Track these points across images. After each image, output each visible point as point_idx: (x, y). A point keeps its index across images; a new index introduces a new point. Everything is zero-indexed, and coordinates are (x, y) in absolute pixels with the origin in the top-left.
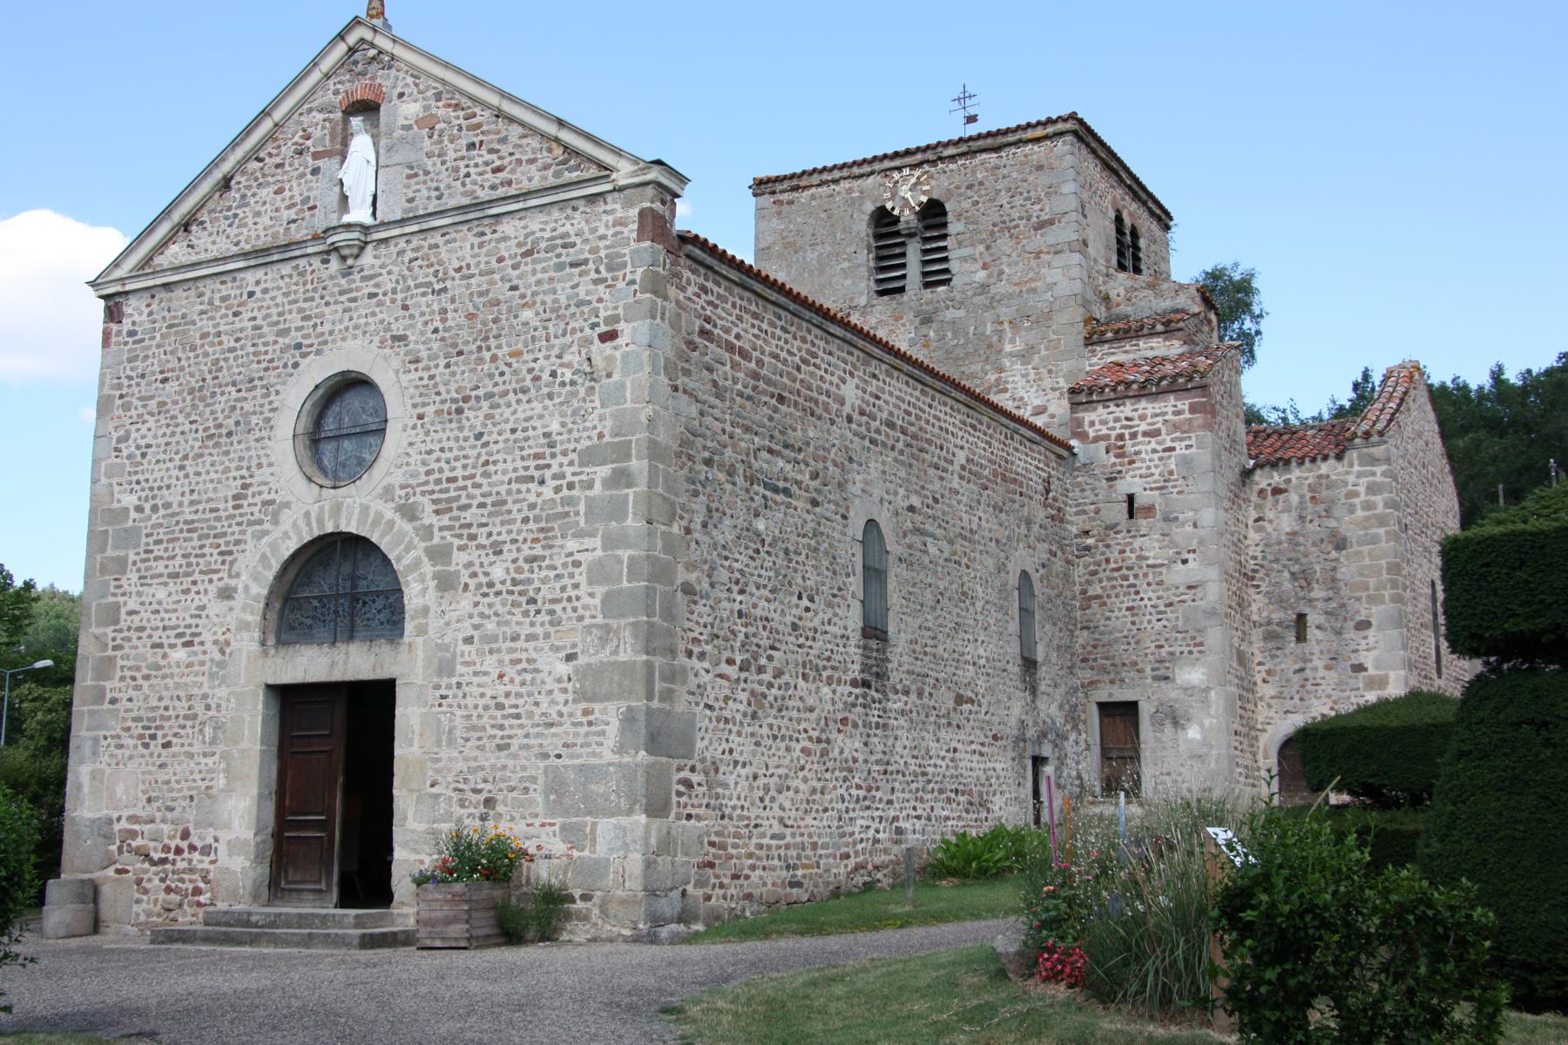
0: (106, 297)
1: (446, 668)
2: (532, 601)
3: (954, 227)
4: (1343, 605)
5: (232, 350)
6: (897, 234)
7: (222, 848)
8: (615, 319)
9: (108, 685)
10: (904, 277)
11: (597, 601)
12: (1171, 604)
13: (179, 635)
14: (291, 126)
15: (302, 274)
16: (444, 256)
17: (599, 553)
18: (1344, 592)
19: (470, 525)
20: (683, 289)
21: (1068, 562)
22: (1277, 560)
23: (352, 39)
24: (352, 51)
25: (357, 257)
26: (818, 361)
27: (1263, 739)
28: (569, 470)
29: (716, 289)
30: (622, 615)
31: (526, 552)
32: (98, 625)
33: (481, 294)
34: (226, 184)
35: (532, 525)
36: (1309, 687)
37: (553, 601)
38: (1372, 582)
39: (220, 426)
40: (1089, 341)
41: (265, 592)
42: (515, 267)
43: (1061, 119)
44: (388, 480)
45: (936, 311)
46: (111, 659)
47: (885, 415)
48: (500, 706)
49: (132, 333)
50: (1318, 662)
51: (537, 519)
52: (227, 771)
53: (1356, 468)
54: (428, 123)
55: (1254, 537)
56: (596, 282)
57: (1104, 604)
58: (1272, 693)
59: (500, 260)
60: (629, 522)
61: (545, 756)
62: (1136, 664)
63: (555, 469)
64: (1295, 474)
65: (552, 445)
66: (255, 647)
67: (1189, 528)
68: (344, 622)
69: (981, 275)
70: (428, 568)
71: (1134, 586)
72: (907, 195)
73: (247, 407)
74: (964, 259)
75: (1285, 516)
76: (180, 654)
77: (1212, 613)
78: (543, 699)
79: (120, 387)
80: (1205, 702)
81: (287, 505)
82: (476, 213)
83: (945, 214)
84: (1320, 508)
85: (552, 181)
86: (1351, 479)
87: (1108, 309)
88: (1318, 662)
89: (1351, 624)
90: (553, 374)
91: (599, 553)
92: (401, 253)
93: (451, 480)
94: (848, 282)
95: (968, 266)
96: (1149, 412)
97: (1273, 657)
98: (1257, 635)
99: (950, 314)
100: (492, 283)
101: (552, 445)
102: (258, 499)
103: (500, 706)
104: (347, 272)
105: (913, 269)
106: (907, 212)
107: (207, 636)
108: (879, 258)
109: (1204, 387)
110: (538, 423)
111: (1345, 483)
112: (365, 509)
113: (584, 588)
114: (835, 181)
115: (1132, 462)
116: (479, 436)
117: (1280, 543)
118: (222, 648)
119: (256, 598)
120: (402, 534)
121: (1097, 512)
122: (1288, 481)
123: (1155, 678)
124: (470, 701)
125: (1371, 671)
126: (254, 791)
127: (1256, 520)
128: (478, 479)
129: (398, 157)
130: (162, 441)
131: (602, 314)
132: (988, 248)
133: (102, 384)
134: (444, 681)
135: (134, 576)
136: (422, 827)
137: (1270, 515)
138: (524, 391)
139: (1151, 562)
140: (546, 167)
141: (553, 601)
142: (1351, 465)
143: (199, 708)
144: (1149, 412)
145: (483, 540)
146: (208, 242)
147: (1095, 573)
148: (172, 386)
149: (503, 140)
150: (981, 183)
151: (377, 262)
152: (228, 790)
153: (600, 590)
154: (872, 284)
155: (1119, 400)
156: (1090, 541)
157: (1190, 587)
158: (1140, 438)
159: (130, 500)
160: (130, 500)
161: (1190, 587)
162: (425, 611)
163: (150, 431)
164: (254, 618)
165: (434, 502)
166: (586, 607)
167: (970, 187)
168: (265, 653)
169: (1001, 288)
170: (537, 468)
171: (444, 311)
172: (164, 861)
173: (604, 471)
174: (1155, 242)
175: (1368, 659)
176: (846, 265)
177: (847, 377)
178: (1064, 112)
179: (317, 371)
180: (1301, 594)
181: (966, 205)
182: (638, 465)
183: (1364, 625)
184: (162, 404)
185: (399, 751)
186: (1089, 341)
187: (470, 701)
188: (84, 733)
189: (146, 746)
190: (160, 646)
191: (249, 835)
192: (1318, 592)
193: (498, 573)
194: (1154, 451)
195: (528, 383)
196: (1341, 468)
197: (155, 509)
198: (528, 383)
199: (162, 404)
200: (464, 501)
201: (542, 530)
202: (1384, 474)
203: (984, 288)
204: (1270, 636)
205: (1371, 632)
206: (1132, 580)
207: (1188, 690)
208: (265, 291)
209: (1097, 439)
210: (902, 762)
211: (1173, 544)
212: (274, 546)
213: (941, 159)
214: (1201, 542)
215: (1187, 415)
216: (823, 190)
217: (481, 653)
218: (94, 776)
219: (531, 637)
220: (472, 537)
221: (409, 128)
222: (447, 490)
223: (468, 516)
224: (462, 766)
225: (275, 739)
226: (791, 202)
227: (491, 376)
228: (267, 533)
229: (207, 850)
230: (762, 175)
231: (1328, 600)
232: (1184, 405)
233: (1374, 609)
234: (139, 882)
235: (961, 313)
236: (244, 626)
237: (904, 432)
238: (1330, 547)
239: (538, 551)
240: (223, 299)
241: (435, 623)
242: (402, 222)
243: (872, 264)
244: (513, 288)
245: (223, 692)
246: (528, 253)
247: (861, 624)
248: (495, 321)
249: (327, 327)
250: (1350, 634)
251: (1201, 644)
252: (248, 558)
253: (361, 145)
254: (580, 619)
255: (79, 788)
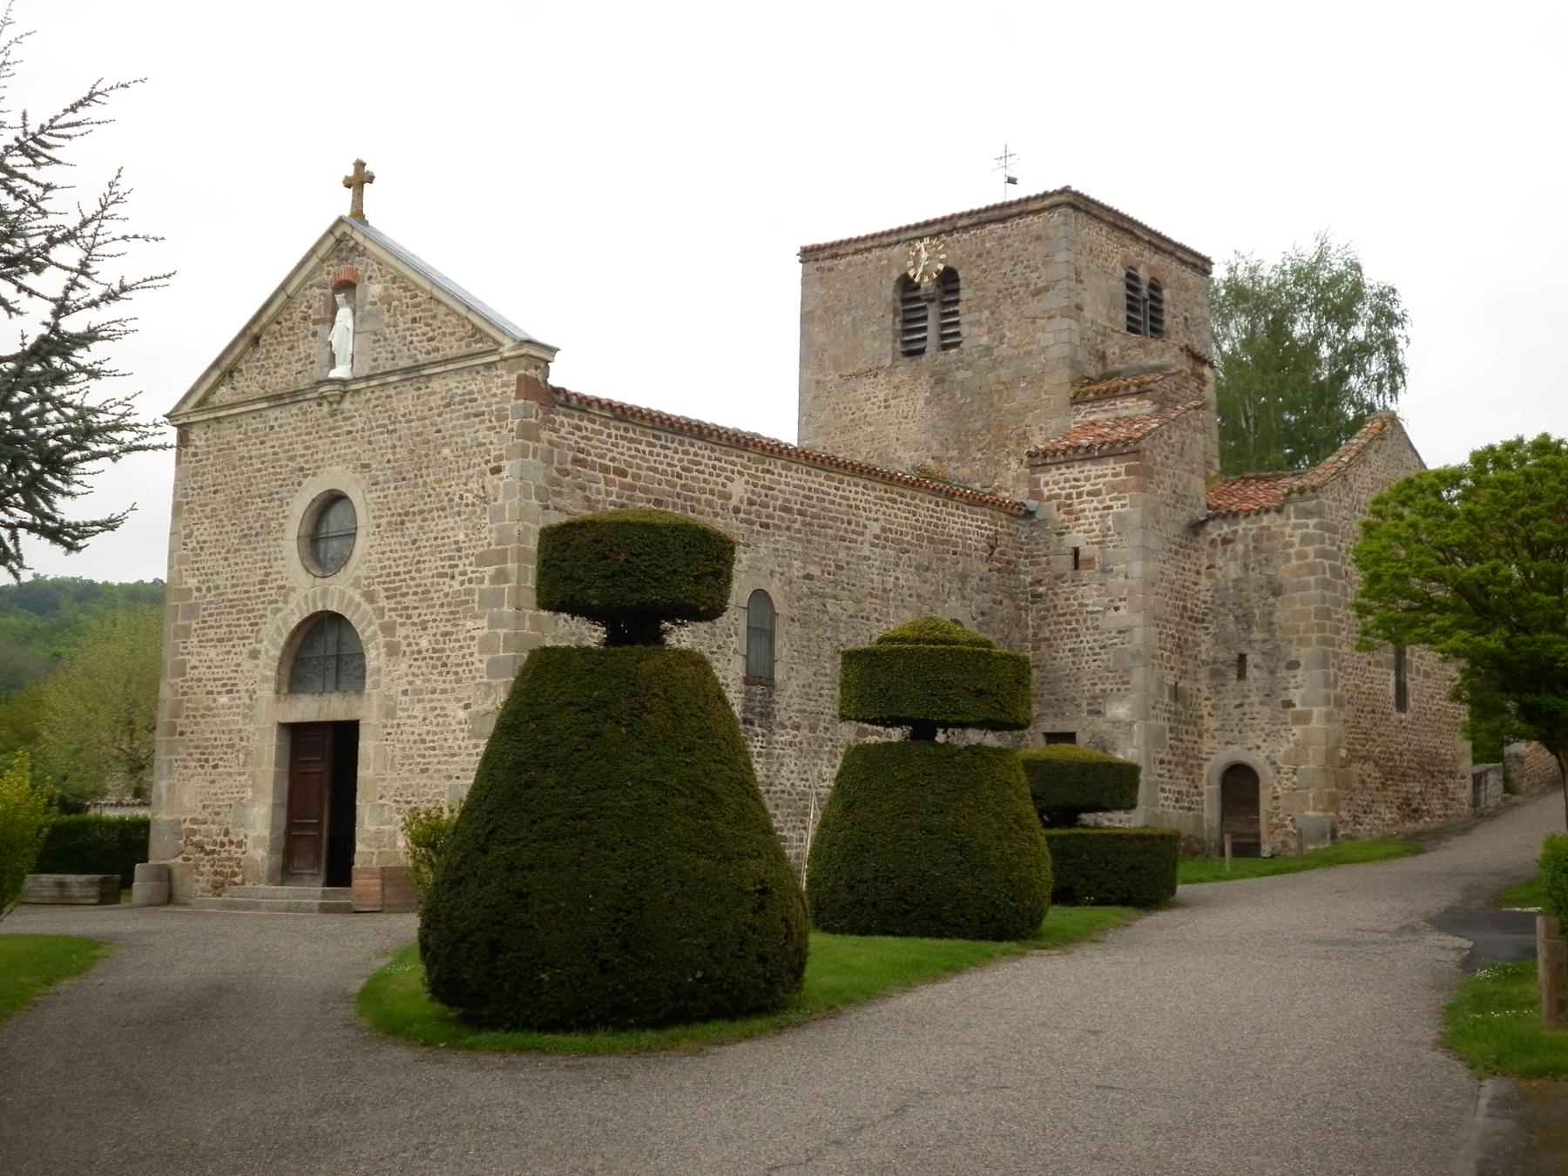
0: (178, 426)
1: (390, 713)
2: (444, 665)
3: (966, 293)
4: (1277, 647)
5: (259, 470)
6: (918, 299)
7: (249, 842)
8: (499, 458)
9: (179, 721)
10: (925, 339)
11: (484, 666)
12: (1104, 647)
13: (224, 685)
14: (299, 299)
15: (304, 414)
16: (395, 404)
17: (486, 631)
18: (1279, 634)
19: (407, 608)
20: (556, 431)
21: (1019, 608)
22: (1223, 605)
23: (338, 234)
24: (339, 241)
25: (339, 403)
26: (701, 468)
27: (1206, 767)
28: (469, 569)
29: (590, 426)
30: (498, 677)
31: (442, 629)
32: (173, 676)
33: (418, 435)
34: (256, 340)
35: (446, 609)
36: (1247, 721)
37: (458, 665)
38: (1302, 625)
39: (250, 528)
40: (1076, 401)
41: (278, 654)
42: (440, 415)
43: (1055, 193)
44: (358, 573)
45: (949, 371)
46: (180, 702)
47: (779, 503)
48: (423, 741)
49: (195, 455)
50: (1255, 699)
51: (449, 604)
52: (253, 786)
53: (1293, 520)
54: (387, 299)
55: (1205, 582)
56: (490, 429)
57: (1051, 646)
58: (1216, 725)
59: (430, 409)
60: (505, 608)
61: (450, 777)
62: (1074, 699)
63: (461, 568)
64: (1242, 526)
65: (459, 550)
66: (271, 694)
67: (1121, 579)
68: (331, 676)
69: (985, 340)
70: (381, 639)
71: (1074, 630)
72: (925, 263)
73: (269, 514)
74: (972, 324)
75: (1232, 565)
76: (223, 699)
77: (1136, 655)
78: (449, 736)
79: (186, 496)
80: (1130, 734)
81: (293, 589)
82: (413, 373)
83: (958, 280)
84: (1262, 556)
85: (464, 351)
86: (1288, 530)
87: (1105, 366)
88: (1255, 699)
89: (1282, 664)
90: (461, 497)
91: (486, 631)
92: (368, 401)
93: (397, 574)
94: (877, 344)
95: (975, 330)
96: (1092, 474)
97: (1218, 692)
98: (1204, 673)
99: (960, 375)
100: (425, 426)
101: (459, 550)
102: (275, 585)
103: (423, 741)
104: (333, 414)
105: (932, 334)
106: (926, 279)
107: (241, 687)
108: (906, 321)
109: (1137, 452)
110: (450, 534)
111: (1283, 534)
112: (343, 593)
113: (477, 656)
114: (869, 250)
115: (1077, 519)
116: (414, 542)
117: (1227, 589)
118: (252, 694)
119: (272, 659)
120: (366, 613)
121: (1048, 563)
122: (1235, 532)
123: (1090, 712)
124: (405, 737)
125: (1299, 708)
126: (270, 801)
127: (1209, 568)
128: (413, 574)
129: (367, 327)
130: (213, 538)
131: (493, 453)
132: (992, 313)
133: (175, 493)
134: (389, 722)
135: (195, 640)
136: (373, 828)
137: (1220, 563)
138: (443, 509)
139: (1090, 609)
140: (462, 339)
141: (458, 665)
142: (1288, 518)
143: (236, 740)
144: (1092, 474)
145: (415, 620)
146: (249, 383)
147: (1044, 618)
148: (220, 497)
149: (434, 317)
150: (989, 252)
151: (353, 407)
152: (254, 800)
153: (486, 658)
154: (898, 345)
155: (1069, 463)
156: (1041, 589)
157: (1120, 632)
158: (1085, 498)
159: (193, 582)
160: (193, 582)
161: (1120, 632)
162: (378, 670)
163: (205, 531)
164: (271, 674)
165: (386, 590)
166: (477, 670)
167: (979, 256)
168: (278, 700)
169: (1003, 351)
170: (451, 566)
171: (394, 447)
172: (213, 852)
173: (490, 570)
174: (1187, 289)
175: (1296, 696)
176: (875, 328)
177: (736, 476)
178: (1058, 187)
179: (313, 489)
180: (1243, 635)
181: (975, 273)
182: (511, 566)
183: (1294, 665)
184: (214, 510)
185: (361, 773)
186: (1076, 401)
187: (405, 737)
188: (163, 757)
189: (202, 767)
190: (211, 693)
191: (266, 833)
192: (1257, 635)
193: (424, 643)
194: (1096, 509)
195: (446, 503)
196: (1279, 520)
197: (209, 590)
198: (446, 503)
199: (214, 510)
200: (404, 590)
201: (451, 613)
202: (1316, 526)
203: (988, 350)
204: (1215, 674)
205: (1299, 672)
206: (1074, 625)
207: (1116, 723)
208: (281, 426)
209: (1050, 498)
210: (788, 784)
211: (1108, 593)
212: (285, 620)
213: (955, 229)
214: (1130, 592)
215: (1123, 477)
216: (859, 258)
217: (412, 702)
218: (170, 788)
219: (444, 691)
220: (409, 617)
221: (374, 304)
222: (393, 582)
223: (408, 601)
224: (398, 784)
225: (286, 763)
226: (831, 269)
227: (422, 497)
228: (280, 610)
229: (240, 844)
230: (808, 243)
231: (1264, 641)
232: (1121, 468)
233: (1303, 651)
234: (197, 867)
235: (969, 374)
236: (265, 679)
237: (801, 513)
238: (1268, 594)
239: (449, 629)
240: (255, 431)
241: (385, 680)
242: (369, 378)
243: (898, 326)
244: (439, 431)
245: (251, 728)
246: (448, 405)
247: (742, 674)
248: (427, 455)
249: (321, 455)
250: (1282, 673)
251: (1127, 683)
252: (268, 630)
253: (344, 316)
254: (474, 678)
255: (160, 797)
